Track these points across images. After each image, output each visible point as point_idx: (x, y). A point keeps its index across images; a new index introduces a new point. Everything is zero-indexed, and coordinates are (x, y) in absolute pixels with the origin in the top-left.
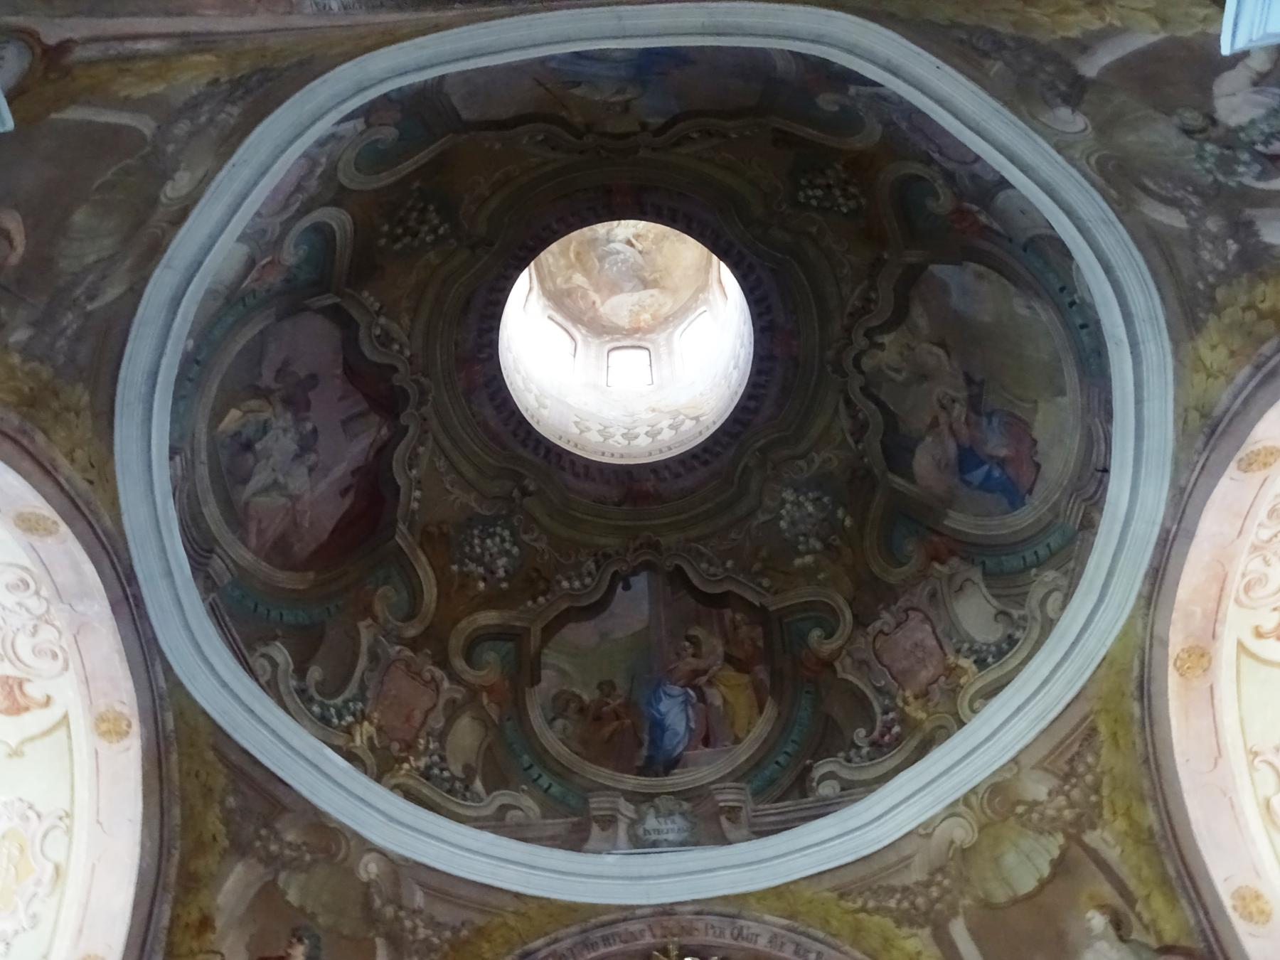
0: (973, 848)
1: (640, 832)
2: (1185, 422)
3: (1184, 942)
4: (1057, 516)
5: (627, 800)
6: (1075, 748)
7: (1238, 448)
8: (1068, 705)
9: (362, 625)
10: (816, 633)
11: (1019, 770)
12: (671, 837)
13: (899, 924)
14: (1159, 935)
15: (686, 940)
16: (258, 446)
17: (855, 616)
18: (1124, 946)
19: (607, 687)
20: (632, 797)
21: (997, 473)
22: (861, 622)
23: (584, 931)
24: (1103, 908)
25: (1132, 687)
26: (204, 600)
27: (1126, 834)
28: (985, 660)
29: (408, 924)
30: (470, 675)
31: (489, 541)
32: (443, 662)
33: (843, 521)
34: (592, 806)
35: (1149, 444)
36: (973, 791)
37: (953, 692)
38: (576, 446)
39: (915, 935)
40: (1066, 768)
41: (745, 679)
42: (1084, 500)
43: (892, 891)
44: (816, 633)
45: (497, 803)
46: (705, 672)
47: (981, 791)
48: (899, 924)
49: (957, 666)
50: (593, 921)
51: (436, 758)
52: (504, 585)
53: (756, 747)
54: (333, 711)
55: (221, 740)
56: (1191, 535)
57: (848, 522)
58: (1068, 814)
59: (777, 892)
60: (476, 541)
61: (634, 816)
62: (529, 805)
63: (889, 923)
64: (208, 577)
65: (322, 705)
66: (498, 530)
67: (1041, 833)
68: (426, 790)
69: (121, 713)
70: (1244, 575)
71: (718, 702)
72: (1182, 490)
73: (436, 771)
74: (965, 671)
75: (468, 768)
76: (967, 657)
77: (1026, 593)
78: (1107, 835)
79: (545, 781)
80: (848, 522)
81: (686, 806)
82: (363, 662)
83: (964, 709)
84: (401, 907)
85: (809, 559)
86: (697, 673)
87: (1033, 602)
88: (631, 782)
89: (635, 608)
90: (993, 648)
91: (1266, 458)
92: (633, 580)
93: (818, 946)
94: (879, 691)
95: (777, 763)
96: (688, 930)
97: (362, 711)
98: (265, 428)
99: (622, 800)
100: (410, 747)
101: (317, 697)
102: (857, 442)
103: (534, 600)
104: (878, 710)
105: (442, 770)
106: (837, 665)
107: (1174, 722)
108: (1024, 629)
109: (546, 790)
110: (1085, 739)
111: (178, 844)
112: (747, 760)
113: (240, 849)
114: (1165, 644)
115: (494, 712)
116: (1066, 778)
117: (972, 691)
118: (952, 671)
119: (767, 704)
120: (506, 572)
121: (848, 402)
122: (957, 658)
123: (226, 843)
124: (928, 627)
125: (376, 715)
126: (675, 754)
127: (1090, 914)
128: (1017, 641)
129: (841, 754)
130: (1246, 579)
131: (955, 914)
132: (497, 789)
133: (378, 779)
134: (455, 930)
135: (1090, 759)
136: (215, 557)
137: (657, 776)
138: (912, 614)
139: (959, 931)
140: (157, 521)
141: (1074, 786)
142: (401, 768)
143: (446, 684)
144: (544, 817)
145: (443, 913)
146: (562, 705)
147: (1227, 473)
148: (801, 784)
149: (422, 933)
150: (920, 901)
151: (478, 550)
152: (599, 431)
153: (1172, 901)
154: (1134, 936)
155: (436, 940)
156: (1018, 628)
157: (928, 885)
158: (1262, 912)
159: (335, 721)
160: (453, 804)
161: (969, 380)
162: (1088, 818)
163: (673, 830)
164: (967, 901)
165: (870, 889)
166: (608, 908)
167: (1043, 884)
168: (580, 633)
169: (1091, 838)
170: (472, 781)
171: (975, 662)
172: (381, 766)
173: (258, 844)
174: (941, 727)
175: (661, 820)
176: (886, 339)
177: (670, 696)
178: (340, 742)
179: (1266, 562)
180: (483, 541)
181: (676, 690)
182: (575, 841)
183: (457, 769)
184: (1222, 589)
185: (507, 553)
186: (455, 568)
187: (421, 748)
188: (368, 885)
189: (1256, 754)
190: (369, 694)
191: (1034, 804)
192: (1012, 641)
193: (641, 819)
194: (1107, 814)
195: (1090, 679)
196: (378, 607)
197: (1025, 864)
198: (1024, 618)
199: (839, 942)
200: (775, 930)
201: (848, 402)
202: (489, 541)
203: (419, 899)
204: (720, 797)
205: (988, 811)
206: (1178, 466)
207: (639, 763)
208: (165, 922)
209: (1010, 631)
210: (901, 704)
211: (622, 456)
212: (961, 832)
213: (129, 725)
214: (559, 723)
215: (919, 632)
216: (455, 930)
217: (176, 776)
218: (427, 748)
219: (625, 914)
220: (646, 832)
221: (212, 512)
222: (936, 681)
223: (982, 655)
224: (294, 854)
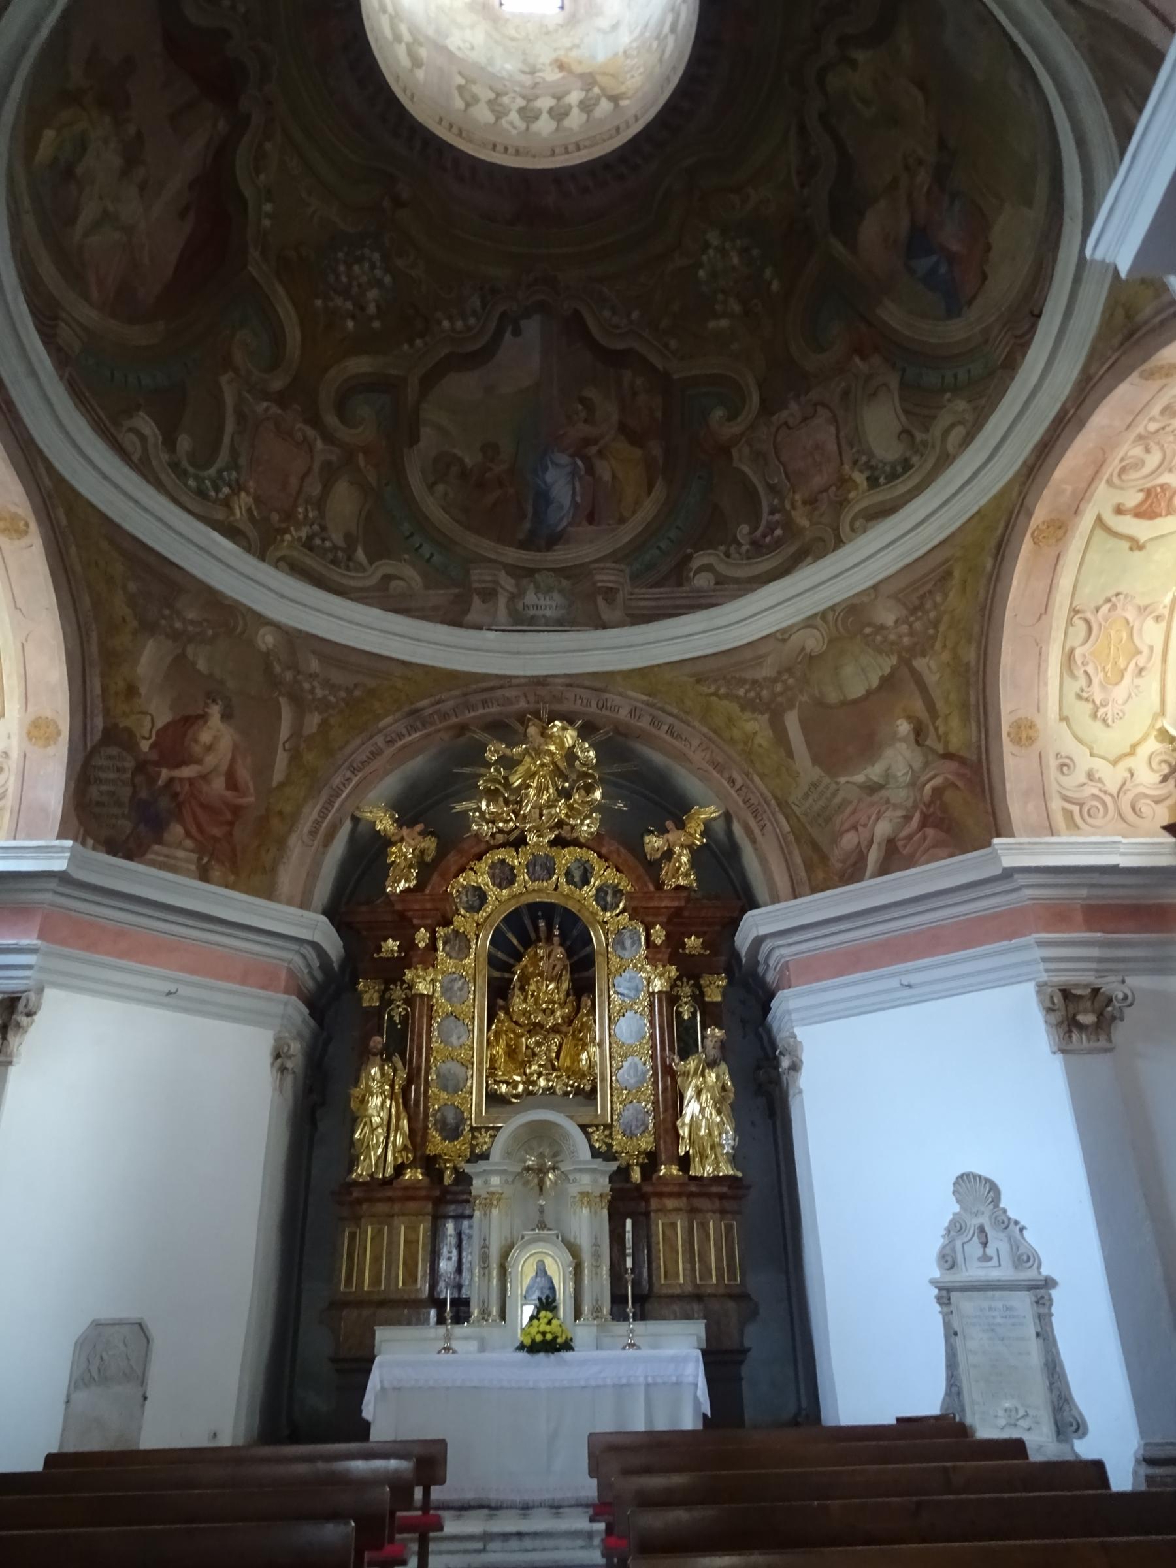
0: (820, 656)
1: (520, 606)
2: (1112, 315)
3: (963, 753)
4: (986, 342)
5: (507, 573)
6: (929, 586)
7: (1144, 361)
8: (935, 547)
9: (224, 379)
10: (718, 413)
11: (876, 597)
12: (548, 613)
13: (743, 709)
14: (947, 743)
15: (557, 707)
16: (79, 170)
17: (763, 401)
18: (918, 749)
19: (490, 450)
20: (515, 571)
21: (943, 269)
22: (768, 408)
23: (465, 695)
24: (909, 718)
25: (993, 543)
26: (61, 378)
27: (948, 664)
28: (877, 479)
29: (307, 686)
30: (345, 434)
31: (356, 268)
32: (315, 421)
33: (770, 283)
34: (474, 578)
35: (1075, 324)
36: (832, 608)
37: (841, 504)
38: (460, 134)
39: (756, 719)
40: (917, 603)
41: (638, 453)
42: (1016, 337)
43: (742, 682)
44: (718, 413)
45: (379, 574)
46: (596, 442)
47: (838, 609)
48: (743, 709)
49: (850, 478)
50: (474, 687)
51: (316, 527)
52: (376, 324)
53: (640, 529)
54: (208, 482)
55: (113, 531)
56: (1082, 424)
57: (775, 286)
58: (906, 640)
59: (643, 673)
60: (342, 268)
61: (515, 590)
62: (409, 575)
63: (734, 708)
64: (60, 349)
65: (196, 477)
66: (367, 251)
67: (880, 653)
68: (310, 561)
69: (16, 513)
70: (1122, 460)
71: (607, 477)
72: (1090, 378)
73: (318, 541)
74: (856, 486)
75: (348, 537)
76: (861, 471)
77: (934, 417)
78: (933, 664)
79: (426, 551)
80: (775, 286)
81: (565, 583)
82: (230, 426)
83: (845, 529)
84: (299, 672)
85: (724, 323)
86: (587, 442)
87: (937, 431)
88: (512, 555)
89: (524, 357)
90: (888, 469)
91: (1168, 371)
92: (523, 323)
93: (671, 720)
94: (773, 489)
95: (659, 548)
96: (559, 699)
97: (237, 481)
98: (82, 145)
99: (503, 573)
100: (289, 516)
101: (191, 470)
102: (802, 185)
103: (411, 343)
104: (765, 509)
105: (323, 540)
106: (735, 452)
107: (1015, 583)
108: (922, 456)
109: (428, 560)
110: (940, 580)
111: (94, 626)
112: (630, 541)
113: (148, 628)
114: (1030, 515)
115: (372, 477)
116: (914, 611)
117: (857, 508)
118: (843, 482)
119: (658, 484)
120: (378, 307)
121: (802, 129)
122: (852, 470)
123: (135, 624)
124: (833, 429)
125: (251, 484)
126: (559, 528)
127: (899, 722)
128: (912, 466)
129: (722, 548)
130: (1124, 463)
131: (791, 706)
132: (381, 557)
133: (262, 558)
134: (349, 691)
135: (938, 599)
136: (62, 324)
137: (539, 550)
138: (819, 409)
139: (792, 721)
140: (11, 317)
141: (918, 619)
142: (283, 541)
143: (319, 444)
144: (427, 587)
145: (337, 677)
146: (443, 467)
147: (1129, 379)
148: (679, 574)
149: (319, 693)
150: (765, 693)
151: (344, 279)
152: (490, 102)
153: (965, 720)
154: (928, 743)
155: (332, 699)
156: (916, 452)
157: (774, 681)
158: (1029, 738)
159: (213, 493)
160: (335, 575)
161: (942, 144)
162: (922, 647)
163: (551, 607)
164: (804, 698)
165: (724, 678)
166: (485, 677)
167: (869, 693)
168: (463, 386)
169: (919, 663)
170: (355, 550)
171: (868, 479)
172: (261, 541)
173: (163, 622)
174: (821, 539)
175: (540, 595)
176: (860, 56)
177: (557, 465)
178: (220, 514)
179: (1147, 451)
180: (349, 267)
181: (564, 459)
182: (455, 617)
183: (337, 538)
184: (1097, 472)
185: (379, 283)
186: (319, 303)
187: (301, 517)
188: (268, 654)
189: (1077, 612)
190: (243, 461)
191: (882, 627)
192: (907, 465)
193: (521, 594)
194: (938, 646)
195: (960, 529)
196: (238, 357)
197: (859, 676)
198: (925, 444)
199: (689, 718)
200: (639, 705)
201: (802, 129)
202: (356, 268)
203: (314, 665)
204: (598, 577)
205: (841, 629)
206: (1094, 355)
207: (521, 536)
208: (98, 691)
209: (908, 454)
210: (788, 506)
211: (517, 153)
212: (813, 642)
213: (27, 525)
214: (440, 488)
215: (823, 433)
216: (349, 691)
217: (78, 568)
218: (306, 516)
219: (502, 682)
220: (525, 607)
221: (47, 269)
222: (826, 490)
223: (877, 473)
224: (198, 630)
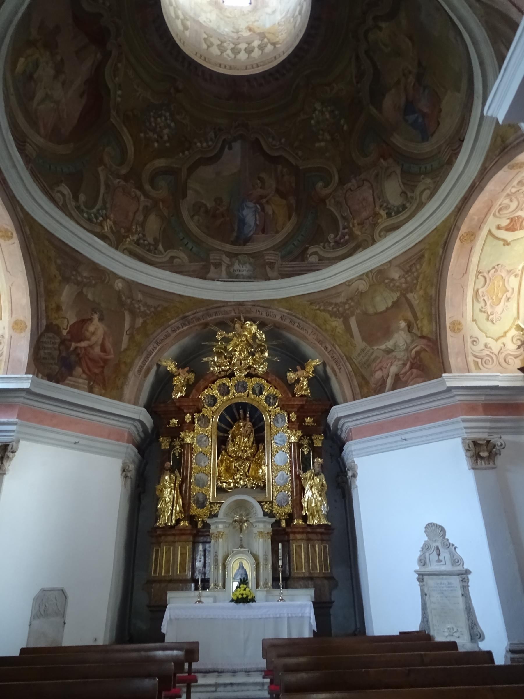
0: (365, 292)
1: (232, 270)
2: (495, 140)
3: (429, 336)
4: (439, 152)
5: (226, 255)
6: (414, 261)
7: (510, 161)
8: (417, 244)
9: (100, 169)
10: (320, 184)
11: (390, 266)
12: (244, 273)
13: (331, 316)
14: (422, 331)
15: (248, 315)
16: (35, 76)
17: (340, 179)
18: (409, 334)
19: (218, 201)
20: (230, 255)
21: (420, 120)
22: (342, 182)
23: (207, 310)
24: (405, 320)
25: (443, 242)
26: (27, 168)
27: (422, 296)
28: (391, 213)
29: (137, 306)
30: (154, 193)
31: (159, 119)
32: (140, 188)
33: (343, 126)
34: (211, 258)
35: (479, 144)
36: (371, 271)
37: (375, 225)
38: (205, 60)
39: (337, 321)
40: (409, 269)
41: (284, 202)
42: (453, 150)
43: (331, 304)
44: (320, 184)
45: (169, 256)
46: (266, 197)
47: (374, 272)
48: (331, 316)
49: (379, 213)
50: (211, 306)
51: (141, 235)
52: (168, 145)
53: (285, 236)
54: (92, 215)
55: (50, 237)
56: (482, 189)
57: (345, 127)
58: (404, 286)
59: (286, 300)
60: (152, 119)
61: (229, 263)
62: (182, 256)
63: (327, 315)
64: (27, 156)
65: (87, 213)
66: (163, 112)
67: (392, 291)
68: (138, 250)
69: (7, 229)
70: (500, 205)
71: (270, 212)
72: (486, 169)
73: (141, 241)
74: (381, 217)
75: (155, 239)
76: (384, 210)
77: (416, 186)
78: (416, 296)
79: (190, 246)
80: (345, 127)
81: (252, 260)
82: (102, 190)
83: (376, 236)
84: (133, 300)
85: (323, 144)
86: (262, 197)
87: (417, 192)
88: (228, 247)
89: (234, 159)
90: (396, 209)
91: (520, 165)
92: (233, 144)
93: (299, 321)
94: (344, 218)
95: (293, 244)
96: (249, 312)
97: (106, 214)
98: (36, 65)
99: (224, 255)
100: (129, 230)
101: (85, 209)
102: (358, 83)
103: (183, 153)
104: (341, 227)
105: (144, 241)
106: (327, 202)
107: (452, 260)
108: (411, 203)
109: (191, 250)
110: (419, 259)
111: (42, 279)
112: (281, 241)
113: (66, 280)
114: (459, 230)
115: (166, 213)
116: (407, 272)
117: (382, 226)
118: (376, 215)
119: (293, 216)
120: (168, 137)
121: (357, 58)
122: (380, 210)
123: (60, 278)
124: (371, 191)
125: (112, 216)
126: (249, 236)
127: (401, 322)
128: (406, 208)
129: (322, 244)
130: (501, 207)
131: (353, 315)
132: (170, 248)
133: (117, 249)
134: (156, 308)
135: (418, 267)
136: (28, 145)
137: (240, 245)
138: (365, 182)
139: (353, 322)
140: (5, 141)
141: (409, 276)
142: (126, 241)
143: (142, 198)
144: (190, 262)
145: (150, 302)
146: (198, 208)
147: (503, 169)
148: (302, 256)
149: (142, 309)
150: (341, 309)
151: (153, 124)
152: (218, 45)
153: (430, 321)
154: (413, 331)
155: (148, 312)
156: (408, 201)
157: (345, 303)
158: (459, 329)
159: (95, 220)
160: (149, 256)
161: (420, 64)
162: (411, 289)
163: (245, 270)
164: (358, 311)
165: (323, 302)
166: (216, 302)
167: (387, 309)
168: (206, 172)
169: (410, 296)
170: (158, 245)
171: (387, 213)
172: (116, 241)
173: (73, 277)
174: (366, 240)
175: (241, 265)
176: (383, 25)
177: (248, 207)
178: (98, 229)
179: (511, 201)
180: (156, 119)
181: (251, 205)
182: (203, 275)
183: (150, 240)
184: (489, 211)
185: (169, 126)
186: (142, 135)
187: (134, 230)
188: (119, 291)
189: (480, 273)
190: (108, 206)
191: (393, 280)
192: (404, 207)
193: (232, 265)
194: (418, 288)
195: (428, 236)
196: (106, 159)
197: (383, 301)
198: (412, 198)
199: (307, 320)
200: (285, 314)
201: (357, 58)
202: (159, 119)
203: (140, 296)
204: (267, 257)
205: (375, 280)
206: (487, 158)
207: (232, 239)
208: (44, 308)
209: (405, 202)
210: (351, 226)
211: (231, 68)
212: (362, 286)
213: (12, 234)
214: (196, 218)
215: (367, 193)
216: (156, 308)
217: (35, 253)
218: (136, 230)
219: (224, 304)
220: (234, 270)
221: (21, 120)
222: (368, 218)
223: (391, 211)
224: (88, 281)
